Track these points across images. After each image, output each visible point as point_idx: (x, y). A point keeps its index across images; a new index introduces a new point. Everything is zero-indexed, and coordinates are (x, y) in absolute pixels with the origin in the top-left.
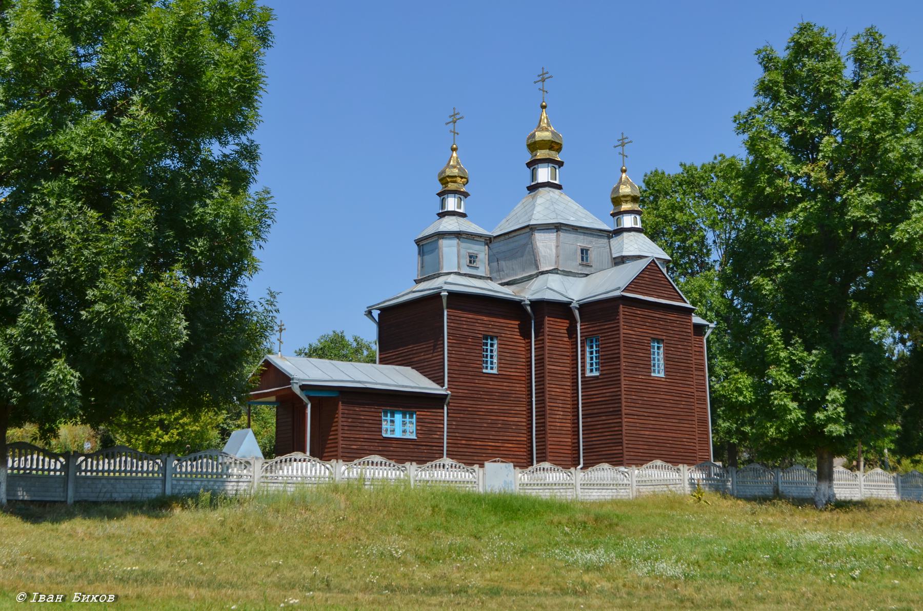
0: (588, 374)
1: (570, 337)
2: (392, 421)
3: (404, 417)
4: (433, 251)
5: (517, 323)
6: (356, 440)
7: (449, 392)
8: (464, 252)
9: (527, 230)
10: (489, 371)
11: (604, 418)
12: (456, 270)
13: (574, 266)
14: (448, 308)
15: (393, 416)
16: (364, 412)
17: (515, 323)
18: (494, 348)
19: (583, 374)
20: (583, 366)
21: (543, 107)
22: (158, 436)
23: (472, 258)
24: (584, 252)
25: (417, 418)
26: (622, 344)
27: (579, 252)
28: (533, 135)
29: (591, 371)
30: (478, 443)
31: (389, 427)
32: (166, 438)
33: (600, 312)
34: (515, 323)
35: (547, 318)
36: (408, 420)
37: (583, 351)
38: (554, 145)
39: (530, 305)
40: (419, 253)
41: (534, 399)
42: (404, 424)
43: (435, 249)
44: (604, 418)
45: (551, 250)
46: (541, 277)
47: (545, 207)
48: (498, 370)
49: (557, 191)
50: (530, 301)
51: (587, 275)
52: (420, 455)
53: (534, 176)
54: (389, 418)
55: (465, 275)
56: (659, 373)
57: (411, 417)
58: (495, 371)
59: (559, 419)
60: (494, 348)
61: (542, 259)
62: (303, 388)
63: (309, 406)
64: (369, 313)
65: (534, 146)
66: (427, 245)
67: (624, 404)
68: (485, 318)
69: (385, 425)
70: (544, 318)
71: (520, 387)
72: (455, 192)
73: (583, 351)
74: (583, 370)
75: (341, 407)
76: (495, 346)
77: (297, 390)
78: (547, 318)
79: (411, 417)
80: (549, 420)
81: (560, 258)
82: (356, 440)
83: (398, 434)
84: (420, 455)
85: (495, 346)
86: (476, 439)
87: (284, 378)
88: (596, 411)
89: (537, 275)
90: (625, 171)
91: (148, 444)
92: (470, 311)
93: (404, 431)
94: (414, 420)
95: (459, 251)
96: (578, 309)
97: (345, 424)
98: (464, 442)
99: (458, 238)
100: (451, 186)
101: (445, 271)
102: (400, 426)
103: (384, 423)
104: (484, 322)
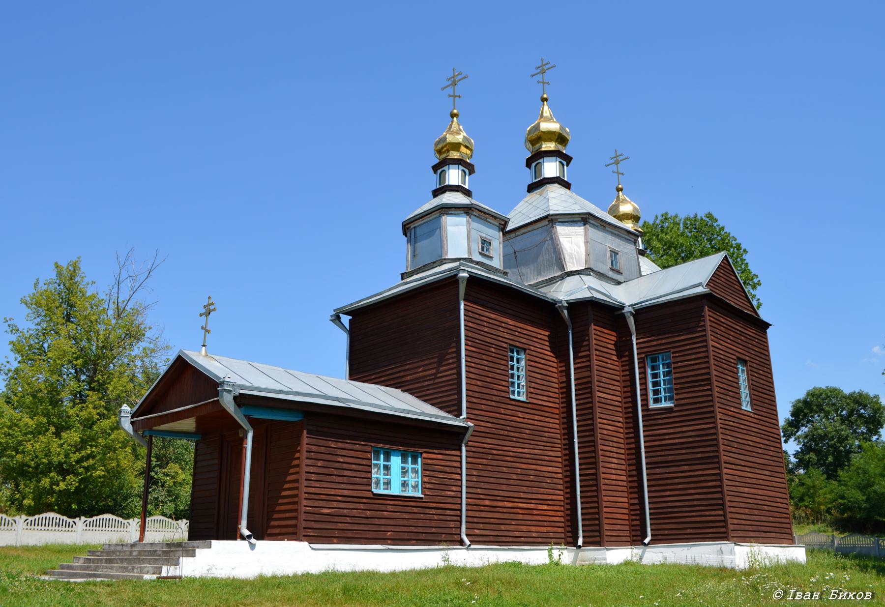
0: (652, 405)
1: (619, 356)
2: (387, 468)
3: (404, 461)
4: (430, 234)
5: (547, 333)
6: (330, 498)
7: (470, 424)
8: (475, 235)
9: (545, 222)
10: (516, 397)
11: (686, 468)
12: (466, 256)
13: (605, 268)
14: (465, 300)
15: (387, 459)
16: (344, 450)
18: (520, 366)
20: (645, 394)
21: (544, 100)
22: (52, 484)
23: (486, 243)
24: (614, 253)
25: (423, 464)
26: (712, 362)
27: (608, 254)
30: (506, 504)
32: (62, 486)
33: (661, 318)
35: (593, 327)
36: (410, 466)
37: (643, 373)
38: (561, 139)
40: (409, 241)
41: (576, 440)
42: (404, 472)
43: (436, 230)
44: (686, 468)
45: (579, 247)
46: (569, 279)
47: (557, 200)
50: (567, 302)
51: (619, 283)
53: (538, 171)
54: (382, 462)
55: (478, 263)
56: (746, 407)
57: (415, 462)
58: (523, 398)
59: (613, 471)
61: (567, 257)
62: (242, 400)
63: (250, 436)
64: (337, 319)
65: (537, 137)
68: (511, 322)
69: (377, 475)
70: (589, 325)
71: (554, 423)
72: (459, 162)
73: (643, 373)
75: (305, 439)
77: (227, 402)
78: (593, 327)
79: (415, 462)
80: (602, 470)
81: (591, 257)
82: (330, 498)
83: (395, 490)
84: (427, 523)
86: (504, 499)
87: (209, 385)
88: (670, 458)
89: (562, 278)
90: (621, 190)
92: (493, 310)
93: (404, 485)
96: (634, 315)
97: (312, 469)
98: (487, 503)
99: (468, 214)
100: (454, 155)
101: (450, 256)
102: (397, 476)
103: (374, 470)
104: (508, 327)
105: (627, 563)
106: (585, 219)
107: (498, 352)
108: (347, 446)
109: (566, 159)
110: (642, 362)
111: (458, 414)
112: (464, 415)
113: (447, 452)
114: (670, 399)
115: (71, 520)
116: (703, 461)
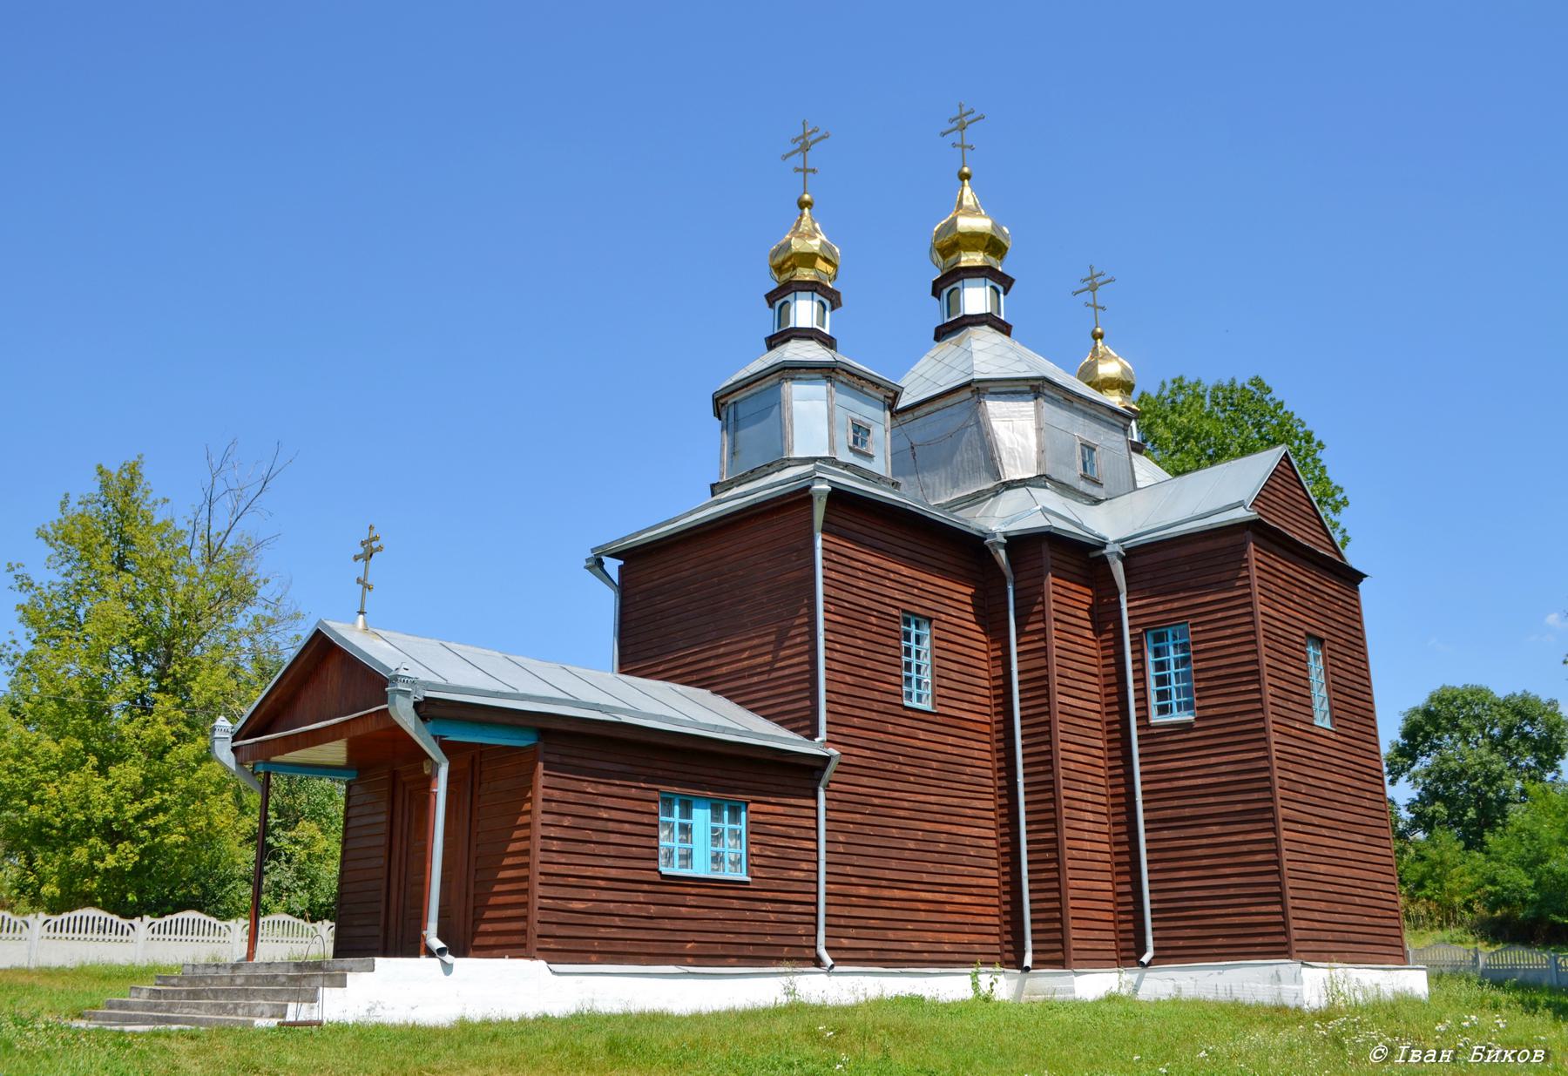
0: (1155, 719)
1: (1098, 630)
2: (686, 829)
3: (717, 817)
4: (763, 414)
5: (970, 591)
6: (584, 882)
7: (833, 751)
8: (842, 416)
9: (966, 394)
10: (915, 704)
11: (1215, 829)
12: (826, 454)
13: (1072, 475)
14: (824, 531)
15: (686, 813)
16: (610, 798)
17: (965, 591)
18: (923, 648)
19: (1143, 717)
20: (1142, 699)
23: (860, 431)
24: (1088, 448)
25: (750, 823)
26: (1262, 641)
27: (1078, 449)
28: (953, 222)
29: (1163, 710)
30: (897, 893)
31: (677, 844)
32: (111, 861)
34: (965, 591)
36: (726, 825)
37: (1140, 661)
38: (994, 246)
39: (1006, 547)
42: (717, 836)
44: (1215, 829)
45: (1026, 438)
47: (987, 354)
48: (934, 705)
49: (999, 337)
51: (1097, 502)
52: (757, 927)
53: (953, 303)
54: (676, 819)
55: (846, 466)
57: (735, 818)
58: (926, 705)
59: (1087, 834)
60: (923, 648)
61: (1004, 455)
62: (428, 709)
64: (597, 564)
65: (953, 243)
66: (743, 405)
67: (1279, 793)
68: (905, 571)
69: (667, 841)
70: (1043, 576)
71: (982, 751)
72: (813, 287)
74: (1143, 709)
76: (926, 643)
77: (403, 714)
79: (735, 818)
80: (1068, 833)
82: (584, 882)
83: (701, 868)
84: (757, 927)
85: (926, 643)
86: (893, 884)
87: (371, 682)
88: (1187, 812)
89: (996, 492)
90: (1101, 336)
91: (70, 877)
93: (717, 859)
94: (742, 827)
95: (831, 411)
96: (1123, 559)
97: (553, 832)
98: (864, 891)
99: (829, 379)
101: (798, 453)
102: (704, 843)
103: (663, 834)
104: (898, 578)
105: (1111, 998)
106: (1036, 388)
107: (883, 623)
108: (615, 790)
109: (1003, 282)
110: (1137, 640)
111: (812, 734)
112: (823, 736)
113: (792, 801)
114: (1188, 706)
115: (126, 922)
116: (1246, 816)
